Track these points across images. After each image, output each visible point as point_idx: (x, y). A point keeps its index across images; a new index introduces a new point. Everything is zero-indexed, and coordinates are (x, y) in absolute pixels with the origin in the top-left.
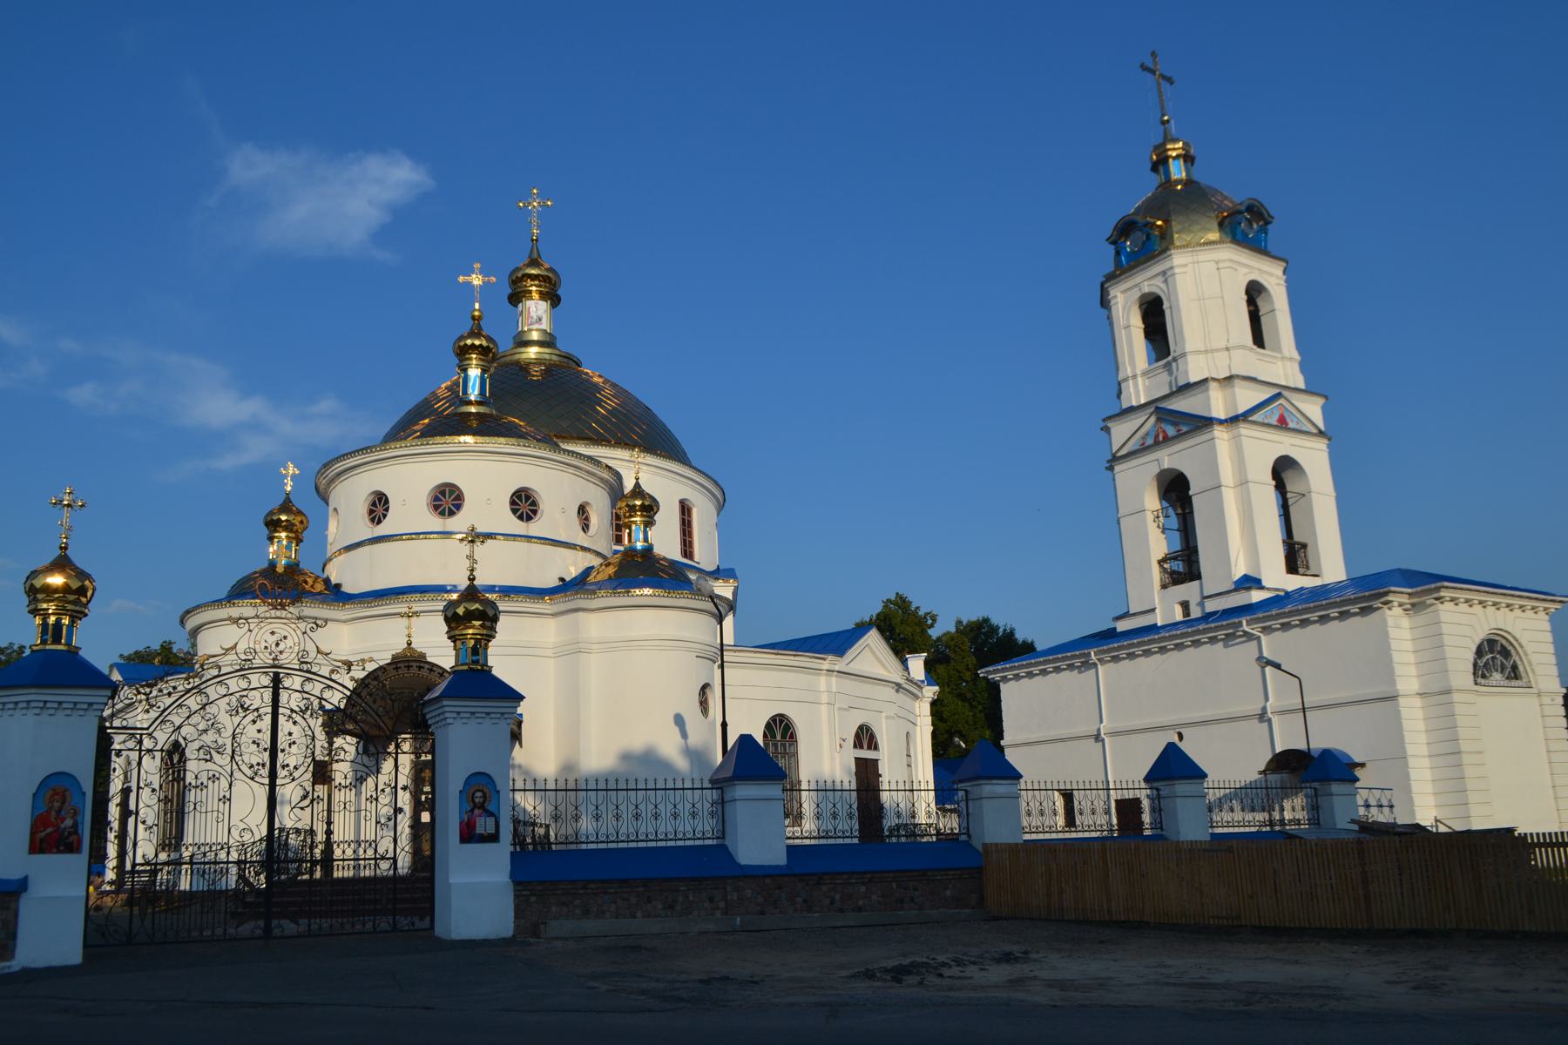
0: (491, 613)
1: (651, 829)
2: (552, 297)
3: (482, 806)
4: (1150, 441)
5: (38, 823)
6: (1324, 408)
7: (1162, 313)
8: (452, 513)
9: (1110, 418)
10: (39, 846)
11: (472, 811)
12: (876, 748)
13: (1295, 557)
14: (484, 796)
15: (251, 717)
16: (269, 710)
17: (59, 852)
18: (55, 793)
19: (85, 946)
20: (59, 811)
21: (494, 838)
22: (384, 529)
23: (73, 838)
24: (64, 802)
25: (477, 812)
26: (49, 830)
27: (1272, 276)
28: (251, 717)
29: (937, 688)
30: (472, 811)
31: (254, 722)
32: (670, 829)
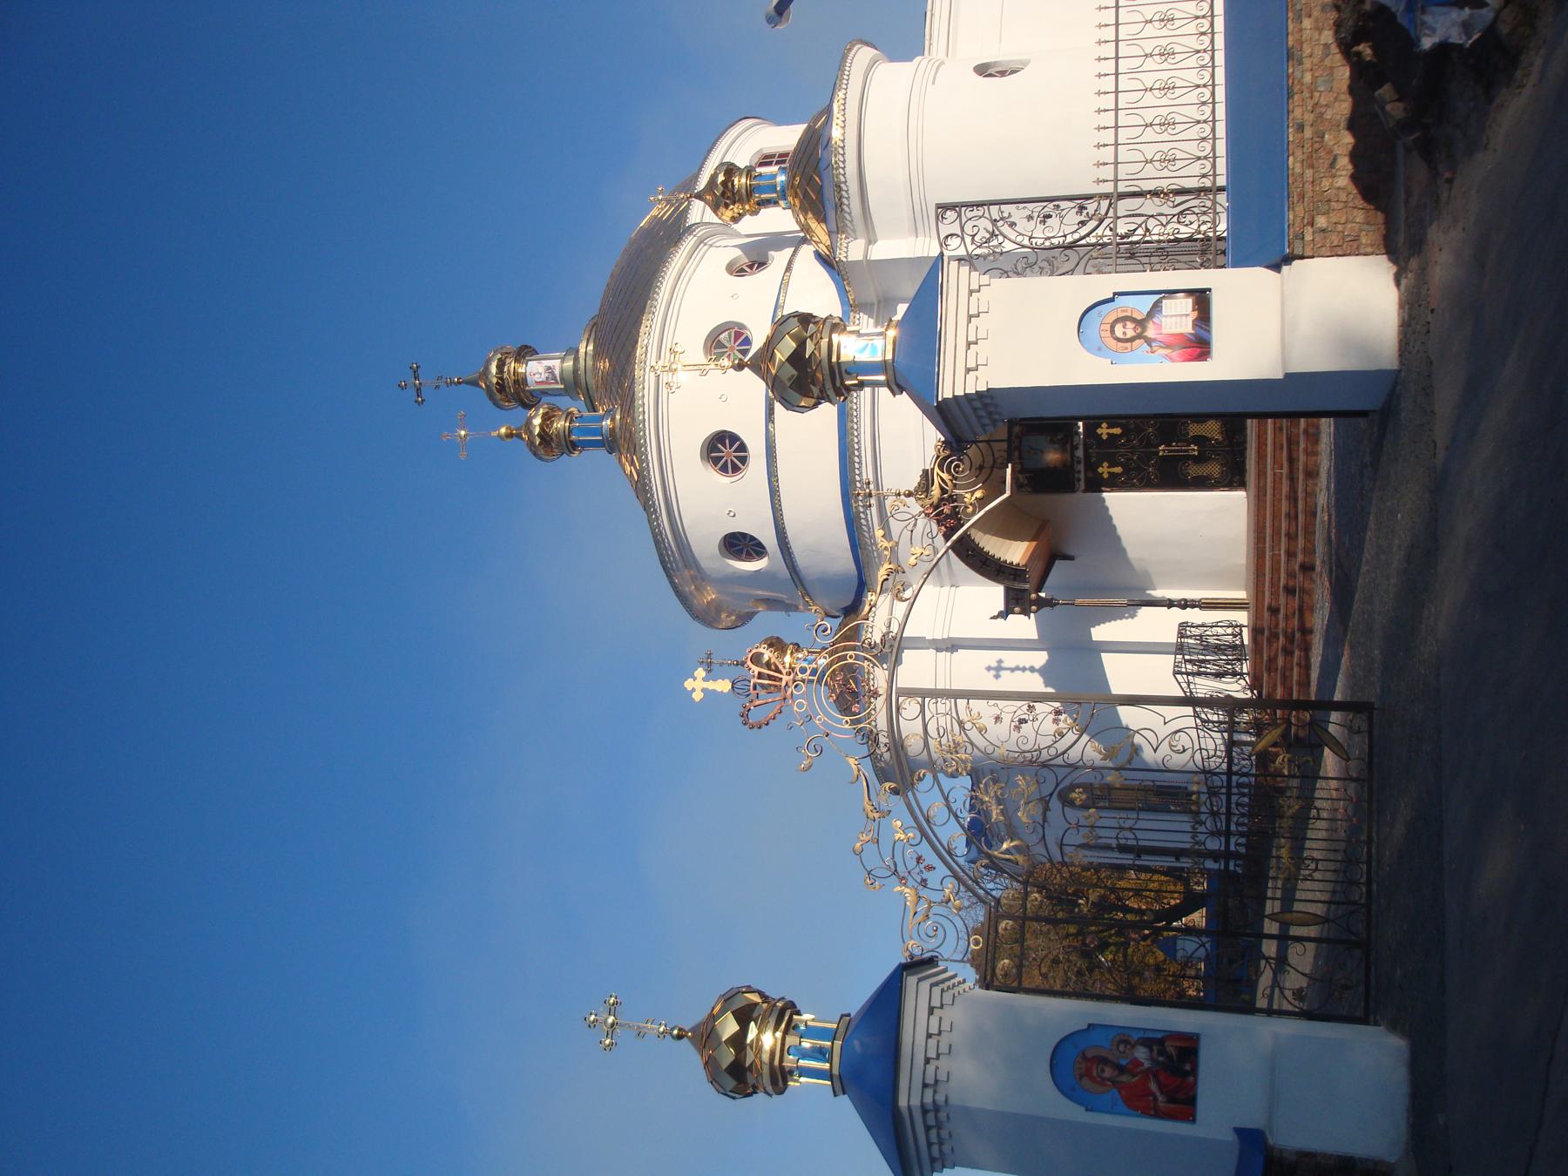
1: (1193, 97)
2: (525, 353)
3: (1141, 324)
5: (1139, 1102)
8: (743, 448)
10: (1182, 1104)
11: (1149, 341)
15: (1006, 229)
16: (962, 703)
17: (1194, 1071)
18: (1088, 1074)
19: (1364, 1021)
20: (1122, 1070)
21: (1201, 298)
22: (768, 538)
23: (1170, 1047)
24: (1104, 1061)
26: (1153, 1086)
28: (1006, 229)
30: (1149, 341)
31: (1012, 225)
32: (1191, 28)
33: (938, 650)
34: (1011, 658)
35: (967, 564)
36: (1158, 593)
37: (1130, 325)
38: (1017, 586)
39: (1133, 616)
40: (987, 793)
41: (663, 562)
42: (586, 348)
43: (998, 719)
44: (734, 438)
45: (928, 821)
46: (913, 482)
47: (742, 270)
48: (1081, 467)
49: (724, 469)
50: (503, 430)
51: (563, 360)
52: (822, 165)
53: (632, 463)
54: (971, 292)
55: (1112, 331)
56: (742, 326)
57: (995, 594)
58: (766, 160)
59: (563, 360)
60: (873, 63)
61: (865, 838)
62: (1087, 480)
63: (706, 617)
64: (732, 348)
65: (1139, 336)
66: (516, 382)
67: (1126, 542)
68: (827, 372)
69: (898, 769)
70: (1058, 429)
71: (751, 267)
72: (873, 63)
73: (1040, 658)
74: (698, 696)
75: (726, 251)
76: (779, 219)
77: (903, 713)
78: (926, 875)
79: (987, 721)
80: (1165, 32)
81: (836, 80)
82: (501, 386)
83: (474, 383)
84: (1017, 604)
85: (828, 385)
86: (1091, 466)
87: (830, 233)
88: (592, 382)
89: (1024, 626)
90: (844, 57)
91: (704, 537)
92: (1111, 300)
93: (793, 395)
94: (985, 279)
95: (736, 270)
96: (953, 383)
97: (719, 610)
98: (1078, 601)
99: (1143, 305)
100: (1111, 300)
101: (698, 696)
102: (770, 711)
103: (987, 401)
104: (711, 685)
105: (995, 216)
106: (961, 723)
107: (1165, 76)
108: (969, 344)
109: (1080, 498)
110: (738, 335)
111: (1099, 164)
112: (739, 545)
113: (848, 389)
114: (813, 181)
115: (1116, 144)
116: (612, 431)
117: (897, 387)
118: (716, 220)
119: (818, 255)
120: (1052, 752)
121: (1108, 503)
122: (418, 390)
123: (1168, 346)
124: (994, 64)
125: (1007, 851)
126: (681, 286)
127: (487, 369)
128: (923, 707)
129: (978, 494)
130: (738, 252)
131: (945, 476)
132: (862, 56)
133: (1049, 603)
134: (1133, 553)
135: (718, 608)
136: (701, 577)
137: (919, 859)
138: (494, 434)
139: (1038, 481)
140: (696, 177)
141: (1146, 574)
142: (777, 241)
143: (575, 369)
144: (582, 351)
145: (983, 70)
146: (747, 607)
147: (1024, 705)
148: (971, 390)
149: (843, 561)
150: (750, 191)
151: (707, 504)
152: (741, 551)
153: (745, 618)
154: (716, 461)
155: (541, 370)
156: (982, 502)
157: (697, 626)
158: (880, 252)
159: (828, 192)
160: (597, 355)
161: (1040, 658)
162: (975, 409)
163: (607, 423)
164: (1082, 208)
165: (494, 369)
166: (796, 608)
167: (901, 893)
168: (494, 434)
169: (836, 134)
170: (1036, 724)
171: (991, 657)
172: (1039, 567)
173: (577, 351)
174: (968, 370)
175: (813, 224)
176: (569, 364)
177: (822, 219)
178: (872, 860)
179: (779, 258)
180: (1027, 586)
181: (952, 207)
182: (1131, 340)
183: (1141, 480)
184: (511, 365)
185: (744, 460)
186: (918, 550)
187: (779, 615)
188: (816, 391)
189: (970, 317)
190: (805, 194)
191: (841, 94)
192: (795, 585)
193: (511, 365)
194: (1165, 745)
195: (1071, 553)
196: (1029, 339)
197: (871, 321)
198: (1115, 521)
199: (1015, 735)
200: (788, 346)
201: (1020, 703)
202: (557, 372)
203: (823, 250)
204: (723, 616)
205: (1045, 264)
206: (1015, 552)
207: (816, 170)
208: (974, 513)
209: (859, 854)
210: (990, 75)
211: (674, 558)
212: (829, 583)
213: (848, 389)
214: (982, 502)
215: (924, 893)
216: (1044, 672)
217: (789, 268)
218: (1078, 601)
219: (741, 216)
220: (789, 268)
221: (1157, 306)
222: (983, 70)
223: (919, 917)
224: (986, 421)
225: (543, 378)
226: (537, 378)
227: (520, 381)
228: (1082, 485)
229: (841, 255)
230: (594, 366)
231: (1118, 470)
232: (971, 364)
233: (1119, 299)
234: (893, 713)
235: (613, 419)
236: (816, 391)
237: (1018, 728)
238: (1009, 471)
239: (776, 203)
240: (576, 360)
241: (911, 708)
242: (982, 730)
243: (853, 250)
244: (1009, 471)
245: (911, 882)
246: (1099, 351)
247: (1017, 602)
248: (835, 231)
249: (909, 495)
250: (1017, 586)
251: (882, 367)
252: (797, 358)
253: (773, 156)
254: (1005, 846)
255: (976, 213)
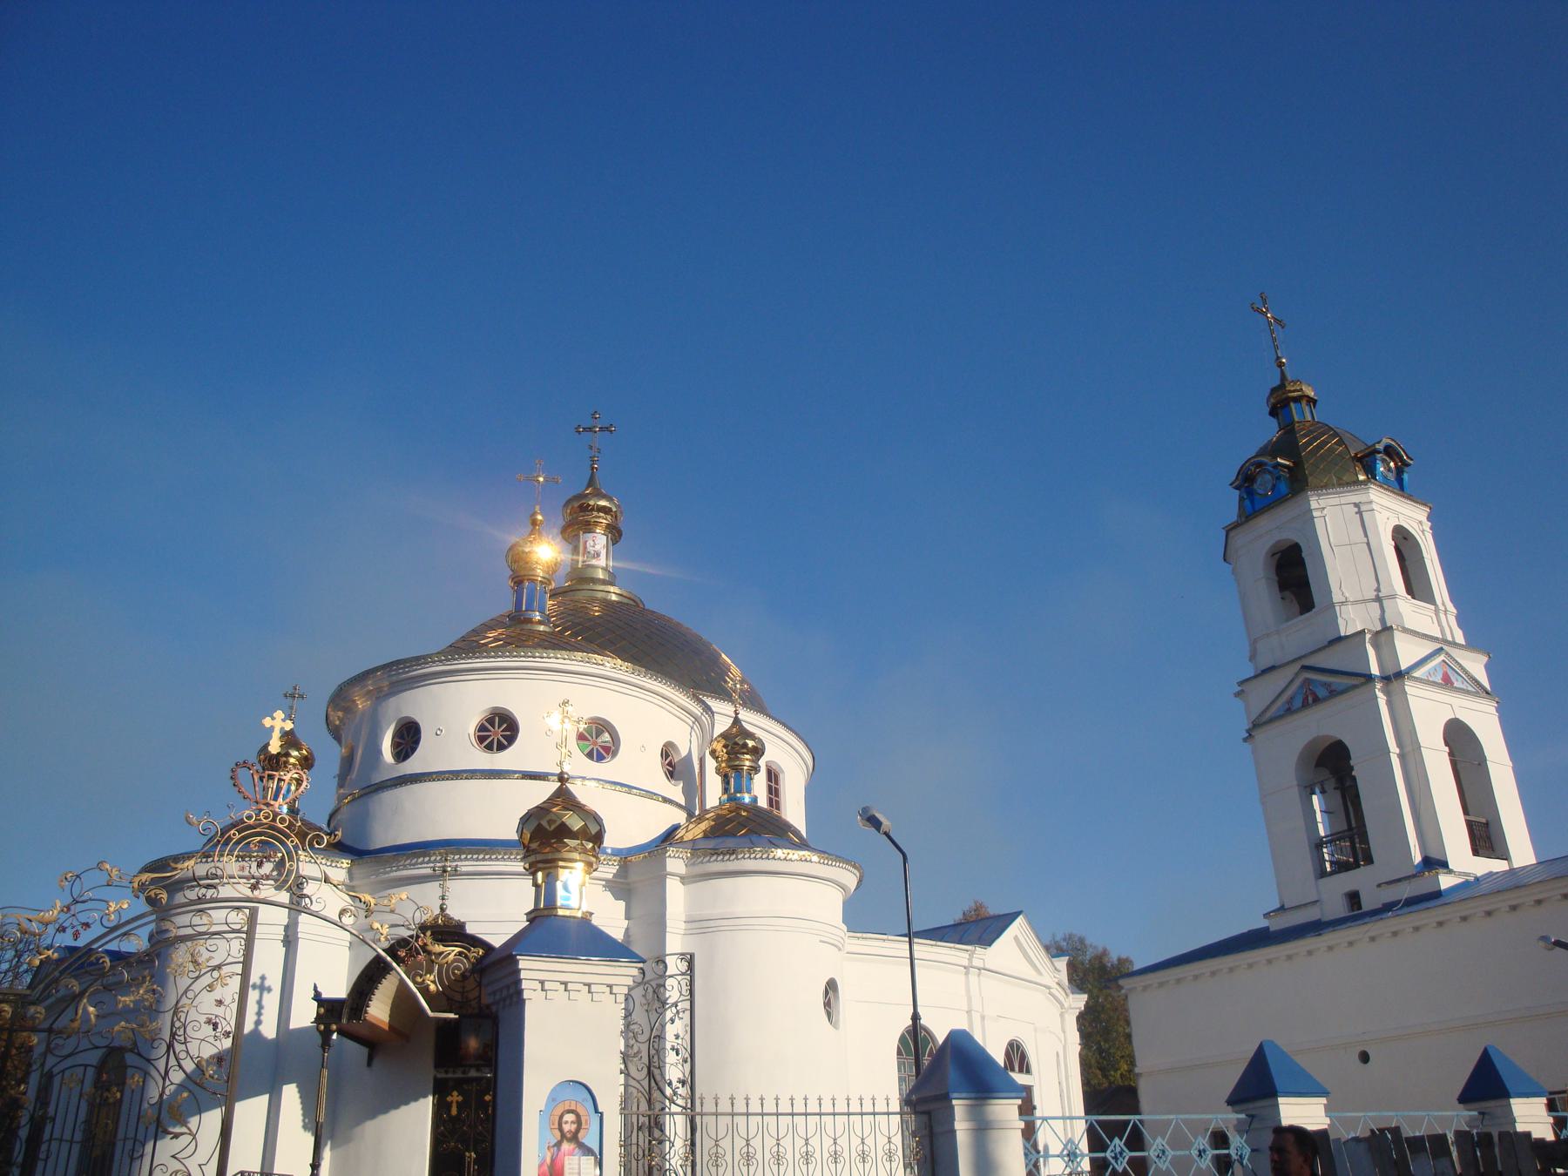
0: (594, 829)
2: (615, 533)
3: (574, 1138)
4: (1298, 703)
6: (1487, 667)
7: (1301, 563)
8: (501, 747)
9: (649, 998)
11: (558, 1144)
12: (1028, 1071)
13: (1486, 838)
14: (579, 1121)
16: (239, 968)
22: (413, 765)
25: (566, 1146)
27: (1415, 518)
29: (1085, 997)
30: (558, 1144)
33: (287, 928)
34: (272, 1002)
35: (363, 973)
36: (327, 1154)
37: (574, 1127)
38: (346, 1011)
39: (305, 1127)
40: (146, 992)
41: (398, 662)
42: (614, 594)
43: (220, 1003)
44: (511, 739)
45: (125, 934)
46: (456, 912)
47: (667, 756)
48: (459, 1075)
49: (482, 728)
50: (539, 517)
51: (605, 569)
52: (754, 838)
53: (496, 640)
54: (610, 986)
55: (569, 1111)
56: (615, 754)
57: (338, 989)
58: (773, 776)
59: (605, 569)
60: (843, 887)
61: (115, 872)
62: (447, 1080)
63: (340, 698)
64: (595, 743)
65: (563, 1135)
66: (588, 523)
67: (382, 1119)
68: (550, 856)
69: (165, 885)
70: (489, 1057)
71: (670, 764)
72: (843, 887)
73: (269, 1030)
74: (267, 722)
75: (687, 742)
76: (714, 793)
77: (234, 914)
78: (70, 931)
79: (218, 993)
80: (854, 1154)
81: (830, 854)
82: (585, 509)
83: (591, 483)
84: (327, 1011)
85: (539, 857)
86: (459, 1085)
87: (693, 841)
88: (580, 596)
89: (304, 1015)
90: (848, 862)
91: (418, 704)
92: (596, 1111)
93: (533, 825)
94: (621, 998)
95: (667, 751)
96: (531, 969)
97: (347, 710)
98: (325, 1072)
99: (590, 1139)
100: (596, 1111)
101: (267, 722)
102: (247, 789)
103: (515, 999)
104: (276, 735)
105: (680, 1006)
106: (218, 967)
107: (789, 1156)
108: (565, 984)
109: (429, 1073)
110: (607, 749)
111: (732, 1099)
112: (408, 738)
113: (534, 874)
114: (742, 830)
115: (733, 1115)
116: (530, 621)
117: (534, 917)
118: (717, 732)
119: (676, 828)
120: (183, 1055)
121: (422, 1101)
122: (590, 429)
123: (553, 1161)
124: (837, 997)
125: (85, 1009)
126: (658, 700)
127: (604, 497)
128: (238, 931)
129: (432, 987)
130: (684, 753)
131: (451, 957)
132: (850, 879)
133: (326, 1035)
134: (371, 1126)
135: (349, 709)
136: (380, 696)
137: (87, 925)
138: (537, 508)
139: (447, 1037)
140: (760, 709)
141: (347, 1140)
142: (694, 789)
143: (595, 581)
144: (612, 589)
145: (831, 986)
146: (347, 736)
147: (231, 1027)
148: (524, 985)
149: (384, 836)
150: (737, 769)
151: (452, 708)
152: (402, 737)
153: (336, 733)
154: (490, 721)
155: (598, 547)
156: (425, 991)
157: (331, 688)
158: (674, 889)
159: (730, 842)
160: (607, 604)
161: (269, 1030)
162: (508, 987)
163: (537, 616)
164: (683, 1083)
165: (603, 503)
166: (341, 785)
167: (54, 907)
168: (537, 508)
169: (779, 853)
170: (211, 1040)
171: (275, 981)
172: (364, 1032)
173: (612, 584)
174: (542, 982)
175: (704, 826)
176: (601, 575)
177: (707, 835)
178: (91, 879)
179: (676, 791)
180: (344, 1021)
181: (691, 967)
182: (560, 1129)
183: (442, 1134)
184: (604, 520)
185: (489, 748)
186: (385, 931)
187: (335, 769)
188: (534, 846)
189: (589, 985)
190: (730, 820)
191: (815, 858)
192: (363, 786)
193: (604, 520)
194: (178, 1166)
195: (376, 1062)
196: (567, 1035)
197: (610, 876)
198: (404, 1109)
199: (203, 1019)
200: (575, 823)
201: (233, 1023)
202: (594, 562)
203: (680, 833)
204: (340, 714)
205: (635, 1049)
206: (379, 1010)
207: (750, 832)
208: (415, 983)
209: (99, 866)
210: (827, 992)
211: (401, 674)
212: (362, 822)
213: (534, 874)
214: (425, 991)
215: (51, 929)
216: (256, 1033)
217: (666, 800)
218: (325, 1072)
219: (716, 758)
220: (666, 800)
221: (588, 1151)
222: (831, 986)
223: (25, 924)
224: (505, 993)
225: (590, 549)
226: (590, 543)
227: (588, 527)
228: (442, 1075)
229: (671, 851)
230: (594, 600)
231: (454, 1111)
232: (547, 985)
233: (596, 1118)
234: (234, 904)
235: (540, 623)
236: (534, 846)
237: (209, 1022)
238: (452, 1016)
239: (726, 790)
240: (604, 582)
241: (238, 919)
242: (210, 988)
243: (676, 863)
244: (452, 1016)
245: (63, 916)
246: (553, 1098)
247: (329, 1010)
248: (694, 847)
249: (442, 910)
250: (346, 1011)
251: (551, 904)
252: (563, 831)
253: (777, 783)
254: (91, 1009)
255: (685, 988)
